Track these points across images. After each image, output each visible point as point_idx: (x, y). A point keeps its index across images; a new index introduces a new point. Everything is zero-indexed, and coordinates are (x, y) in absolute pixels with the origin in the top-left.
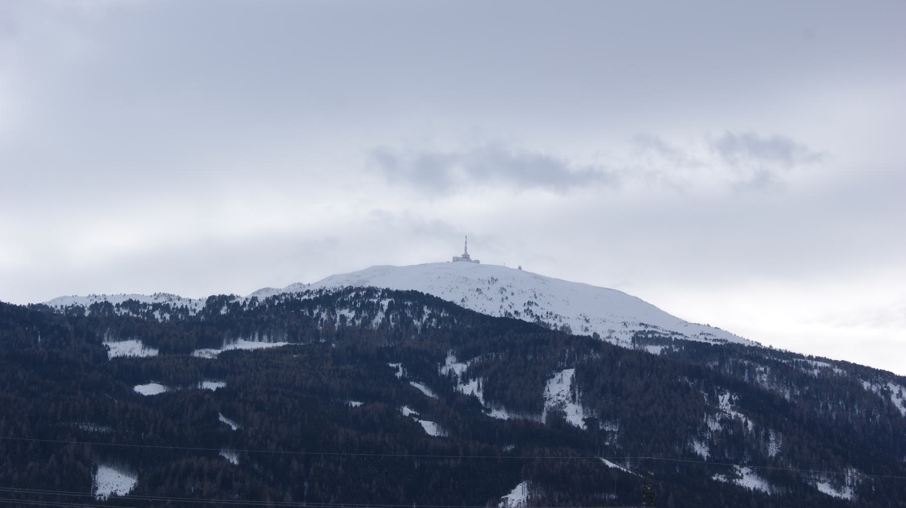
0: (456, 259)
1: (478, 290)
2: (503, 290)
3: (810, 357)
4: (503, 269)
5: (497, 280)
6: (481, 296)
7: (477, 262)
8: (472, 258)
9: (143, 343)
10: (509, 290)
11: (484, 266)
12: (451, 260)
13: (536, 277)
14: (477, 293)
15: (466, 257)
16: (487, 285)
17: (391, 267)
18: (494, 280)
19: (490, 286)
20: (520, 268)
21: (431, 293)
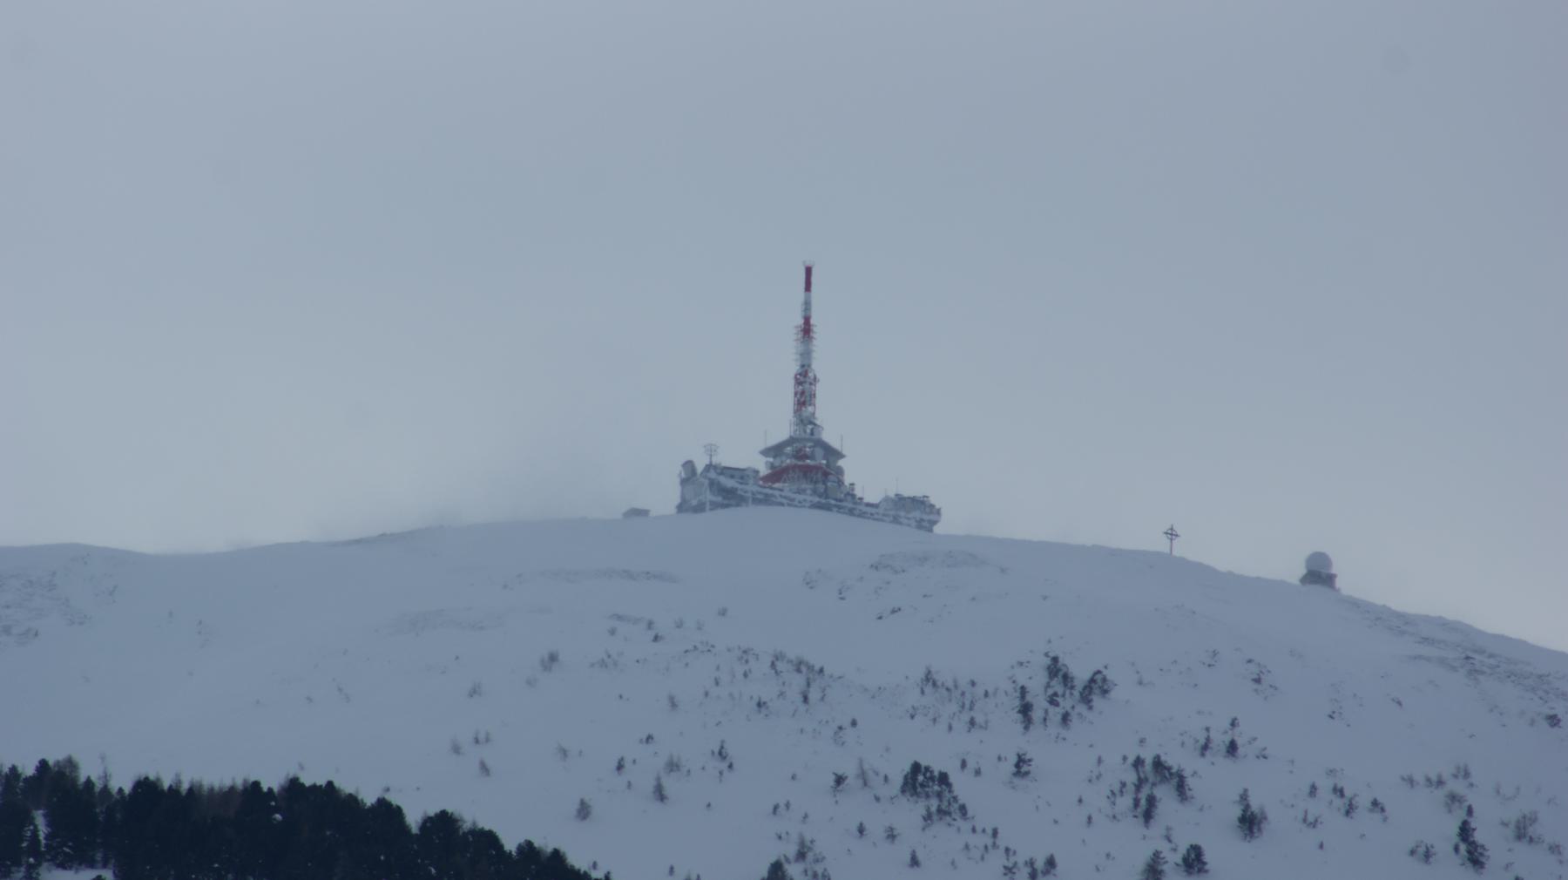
0: (714, 488)
1: (919, 780)
2: (1152, 786)
3: (727, 506)
4: (1170, 583)
5: (1097, 686)
6: (946, 839)
7: (914, 511)
8: (867, 476)
9: (74, 780)
10: (1219, 787)
11: (972, 555)
12: (664, 496)
13: (1474, 657)
14: (908, 814)
15: (807, 468)
16: (1006, 737)
17: (80, 557)
18: (1069, 690)
19: (1037, 744)
20: (1319, 574)
21: (475, 812)
